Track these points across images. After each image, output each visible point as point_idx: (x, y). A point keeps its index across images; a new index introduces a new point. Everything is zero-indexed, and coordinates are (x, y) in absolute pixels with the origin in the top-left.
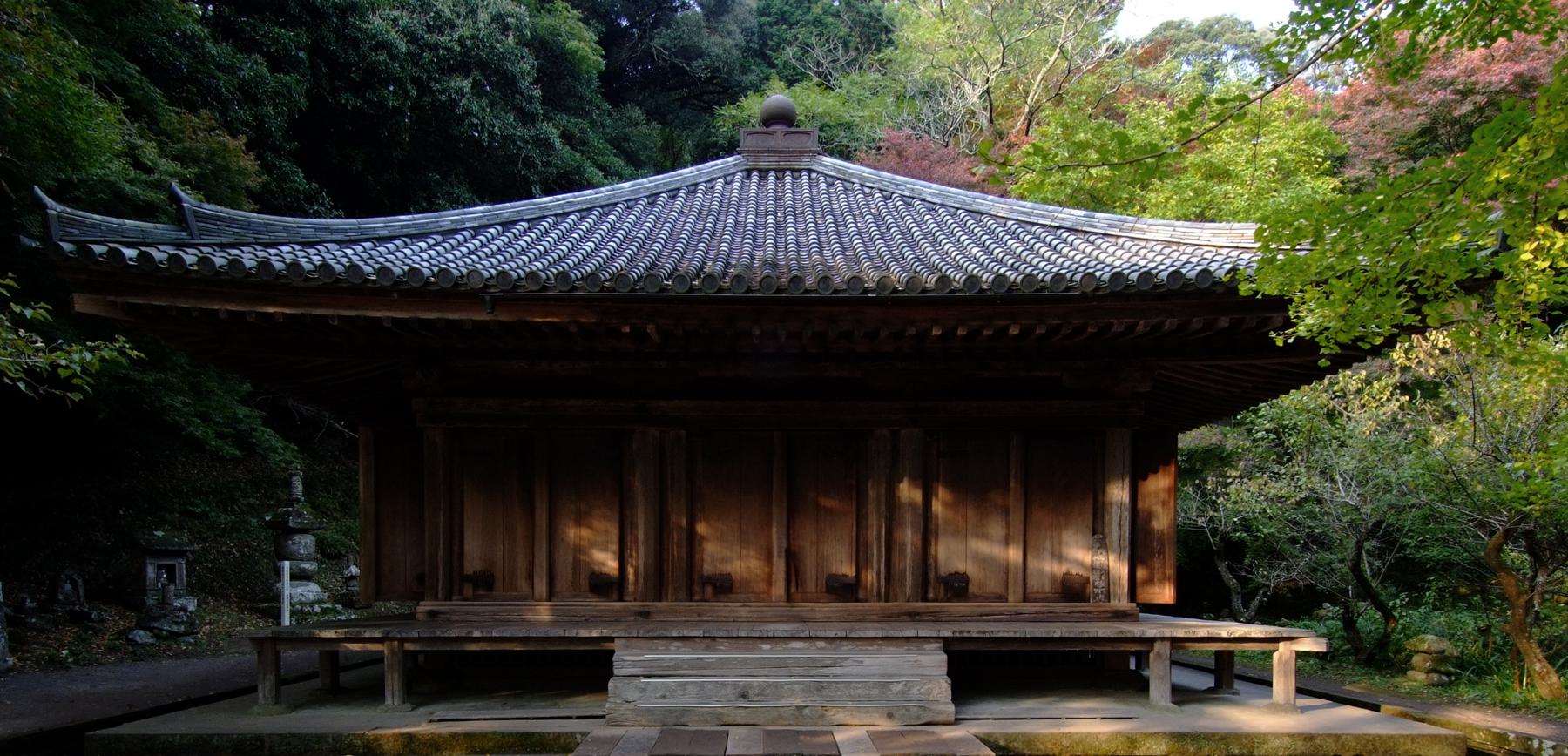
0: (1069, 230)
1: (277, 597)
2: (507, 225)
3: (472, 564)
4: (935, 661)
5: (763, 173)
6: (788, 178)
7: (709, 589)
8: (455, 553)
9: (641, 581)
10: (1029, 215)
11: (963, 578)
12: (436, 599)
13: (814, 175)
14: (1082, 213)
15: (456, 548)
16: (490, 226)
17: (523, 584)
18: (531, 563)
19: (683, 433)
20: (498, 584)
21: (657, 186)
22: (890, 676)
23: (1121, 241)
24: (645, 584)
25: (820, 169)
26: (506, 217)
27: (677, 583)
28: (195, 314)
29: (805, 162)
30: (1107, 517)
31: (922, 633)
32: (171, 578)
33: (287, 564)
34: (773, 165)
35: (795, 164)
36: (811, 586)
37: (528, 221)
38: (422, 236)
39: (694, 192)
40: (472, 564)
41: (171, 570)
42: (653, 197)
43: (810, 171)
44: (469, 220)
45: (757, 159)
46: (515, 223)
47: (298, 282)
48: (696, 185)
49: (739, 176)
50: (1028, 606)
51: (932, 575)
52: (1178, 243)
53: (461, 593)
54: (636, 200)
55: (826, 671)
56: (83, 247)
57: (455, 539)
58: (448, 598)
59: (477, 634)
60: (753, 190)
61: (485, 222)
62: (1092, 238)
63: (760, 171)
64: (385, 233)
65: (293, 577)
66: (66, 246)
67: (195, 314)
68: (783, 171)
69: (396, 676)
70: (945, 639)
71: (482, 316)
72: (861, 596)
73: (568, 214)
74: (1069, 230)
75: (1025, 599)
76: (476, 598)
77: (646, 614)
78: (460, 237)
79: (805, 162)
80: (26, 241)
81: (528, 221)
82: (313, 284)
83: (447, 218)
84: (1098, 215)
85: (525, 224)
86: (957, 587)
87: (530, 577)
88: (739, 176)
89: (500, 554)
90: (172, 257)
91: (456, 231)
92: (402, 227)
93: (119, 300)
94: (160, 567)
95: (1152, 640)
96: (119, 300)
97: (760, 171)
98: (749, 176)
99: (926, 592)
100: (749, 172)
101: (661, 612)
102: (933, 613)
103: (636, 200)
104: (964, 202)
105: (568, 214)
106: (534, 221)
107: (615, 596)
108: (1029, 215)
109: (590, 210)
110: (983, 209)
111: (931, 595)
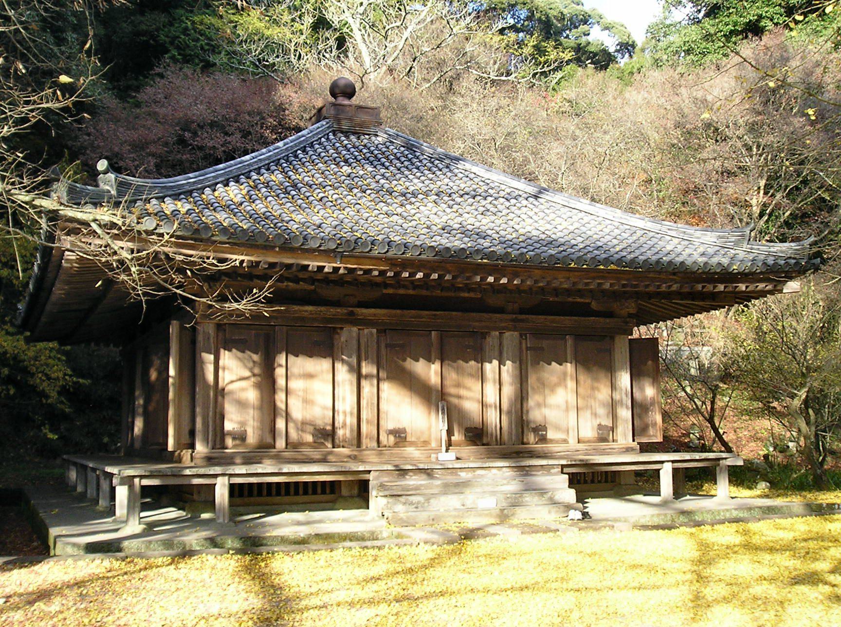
19: (374, 331)
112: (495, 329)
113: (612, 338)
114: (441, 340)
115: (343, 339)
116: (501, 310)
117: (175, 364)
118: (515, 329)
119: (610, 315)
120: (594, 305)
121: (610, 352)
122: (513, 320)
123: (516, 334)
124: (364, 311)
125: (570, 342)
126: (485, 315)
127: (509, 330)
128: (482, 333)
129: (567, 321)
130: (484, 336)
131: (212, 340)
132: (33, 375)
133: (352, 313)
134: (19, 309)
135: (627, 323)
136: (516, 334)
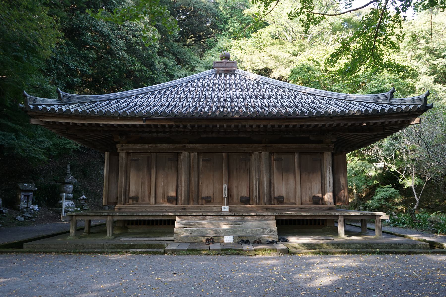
0: (310, 94)
1: (61, 206)
2: (146, 94)
3: (132, 194)
4: (272, 223)
5: (220, 74)
6: (228, 76)
7: (204, 201)
8: (127, 190)
9: (183, 198)
10: (299, 89)
11: (282, 197)
12: (121, 204)
13: (236, 74)
14: (314, 89)
15: (127, 189)
16: (140, 94)
17: (147, 200)
18: (150, 193)
19: (196, 154)
20: (140, 200)
21: (189, 79)
22: (259, 227)
23: (325, 98)
24: (184, 200)
25: (237, 73)
26: (145, 91)
27: (195, 200)
28: (63, 124)
29: (233, 71)
30: (325, 179)
31: (268, 214)
32: (28, 199)
33: (65, 194)
34: (223, 71)
35: (230, 71)
36: (235, 199)
37: (151, 92)
38: (122, 98)
39: (200, 80)
40: (132, 194)
41: (28, 196)
42: (187, 83)
43: (235, 73)
44: (135, 93)
45: (219, 70)
46: (147, 93)
47: (93, 115)
48: (200, 78)
49: (213, 75)
50: (303, 206)
51: (272, 196)
52: (341, 100)
53: (128, 203)
54: (182, 84)
55: (240, 226)
56: (36, 106)
57: (127, 185)
58: (124, 204)
59: (135, 214)
60: (217, 80)
61: (139, 93)
62: (317, 97)
63: (219, 73)
64: (112, 98)
65: (66, 199)
66: (32, 106)
67: (63, 124)
68: (226, 73)
69: (111, 228)
70: (276, 216)
71: (142, 123)
72: (251, 203)
73: (163, 89)
74: (310, 94)
75: (301, 204)
76: (133, 204)
77: (184, 209)
78: (133, 98)
79: (233, 71)
80: (20, 105)
81: (151, 92)
82: (96, 116)
83: (129, 92)
84: (318, 90)
85: (150, 93)
86: (280, 200)
87: (149, 198)
88: (213, 75)
89: (140, 190)
90: (59, 109)
91: (131, 96)
92: (117, 96)
93: (43, 120)
94: (25, 195)
95: (338, 216)
96: (43, 120)
97: (219, 73)
98: (216, 75)
99: (271, 202)
100: (216, 74)
101: (189, 208)
102: (273, 208)
103: (182, 84)
104: (280, 84)
105: (163, 89)
106: (153, 92)
107: (175, 204)
108: (299, 89)
109: (169, 87)
110: (286, 87)
111: (272, 203)
112: (256, 151)
113: (322, 153)
114: (228, 157)
115: (182, 158)
116: (260, 142)
117: (107, 165)
118: (266, 150)
119: (321, 142)
120: (311, 138)
121: (321, 161)
122: (264, 146)
123: (267, 153)
124: (191, 145)
125: (296, 156)
126: (250, 145)
127: (264, 151)
128: (249, 153)
129: (294, 146)
130: (250, 154)
131: (124, 160)
132: (36, 36)
133: (185, 146)
134: (34, 204)
135: (329, 146)
136: (267, 153)
